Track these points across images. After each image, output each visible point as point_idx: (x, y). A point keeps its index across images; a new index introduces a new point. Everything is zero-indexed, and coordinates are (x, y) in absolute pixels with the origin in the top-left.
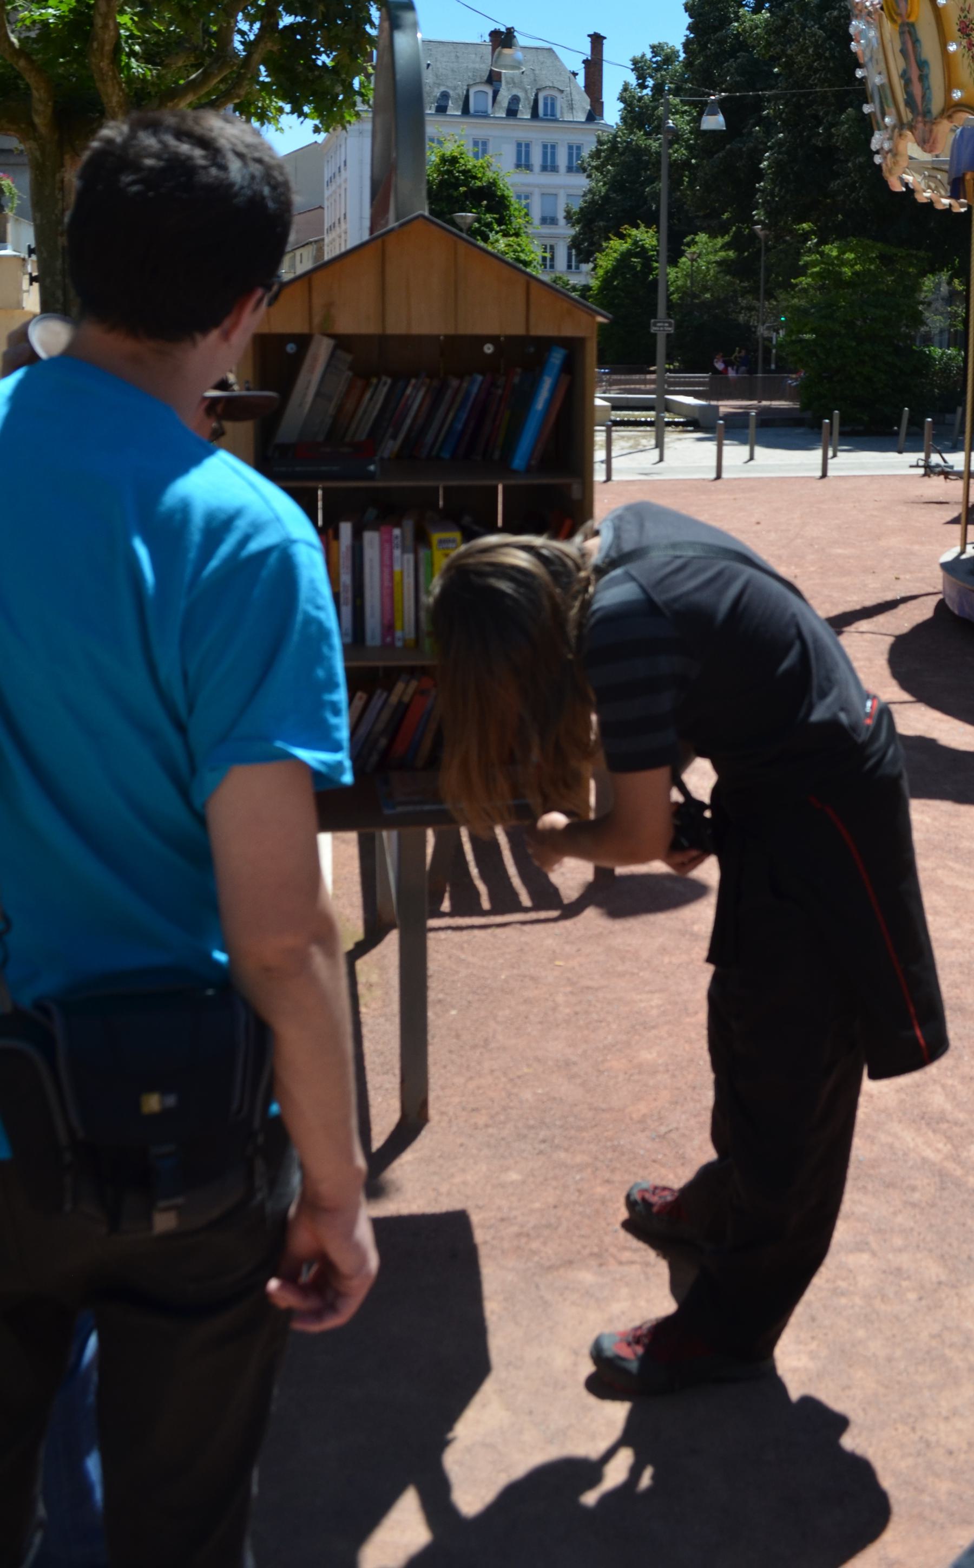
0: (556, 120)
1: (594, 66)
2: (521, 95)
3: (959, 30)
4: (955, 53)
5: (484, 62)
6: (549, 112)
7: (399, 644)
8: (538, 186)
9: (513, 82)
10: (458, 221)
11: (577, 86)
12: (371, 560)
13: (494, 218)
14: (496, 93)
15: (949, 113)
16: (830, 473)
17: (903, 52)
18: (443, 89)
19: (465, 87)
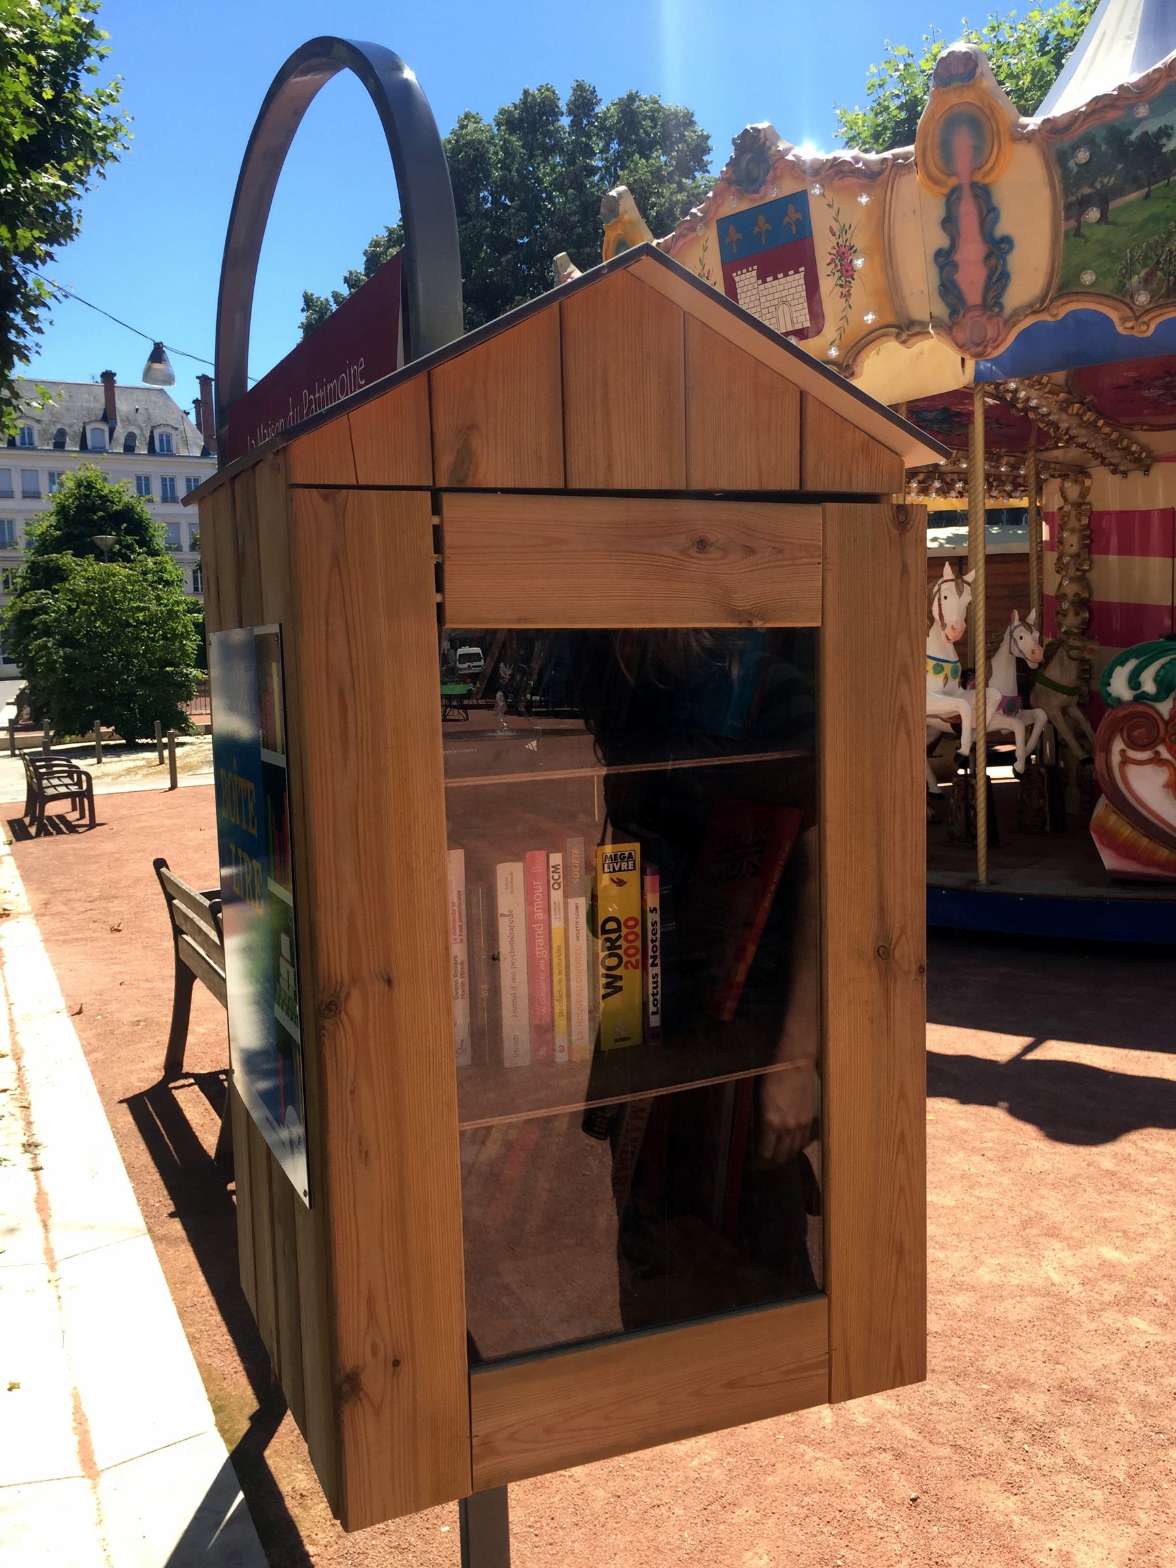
0: (173, 455)
2: (137, 432)
5: (98, 402)
7: (561, 1057)
9: (128, 421)
10: (98, 543)
11: (189, 423)
12: (510, 915)
13: (135, 540)
14: (112, 431)
16: (179, 784)
18: (59, 426)
19: (81, 425)
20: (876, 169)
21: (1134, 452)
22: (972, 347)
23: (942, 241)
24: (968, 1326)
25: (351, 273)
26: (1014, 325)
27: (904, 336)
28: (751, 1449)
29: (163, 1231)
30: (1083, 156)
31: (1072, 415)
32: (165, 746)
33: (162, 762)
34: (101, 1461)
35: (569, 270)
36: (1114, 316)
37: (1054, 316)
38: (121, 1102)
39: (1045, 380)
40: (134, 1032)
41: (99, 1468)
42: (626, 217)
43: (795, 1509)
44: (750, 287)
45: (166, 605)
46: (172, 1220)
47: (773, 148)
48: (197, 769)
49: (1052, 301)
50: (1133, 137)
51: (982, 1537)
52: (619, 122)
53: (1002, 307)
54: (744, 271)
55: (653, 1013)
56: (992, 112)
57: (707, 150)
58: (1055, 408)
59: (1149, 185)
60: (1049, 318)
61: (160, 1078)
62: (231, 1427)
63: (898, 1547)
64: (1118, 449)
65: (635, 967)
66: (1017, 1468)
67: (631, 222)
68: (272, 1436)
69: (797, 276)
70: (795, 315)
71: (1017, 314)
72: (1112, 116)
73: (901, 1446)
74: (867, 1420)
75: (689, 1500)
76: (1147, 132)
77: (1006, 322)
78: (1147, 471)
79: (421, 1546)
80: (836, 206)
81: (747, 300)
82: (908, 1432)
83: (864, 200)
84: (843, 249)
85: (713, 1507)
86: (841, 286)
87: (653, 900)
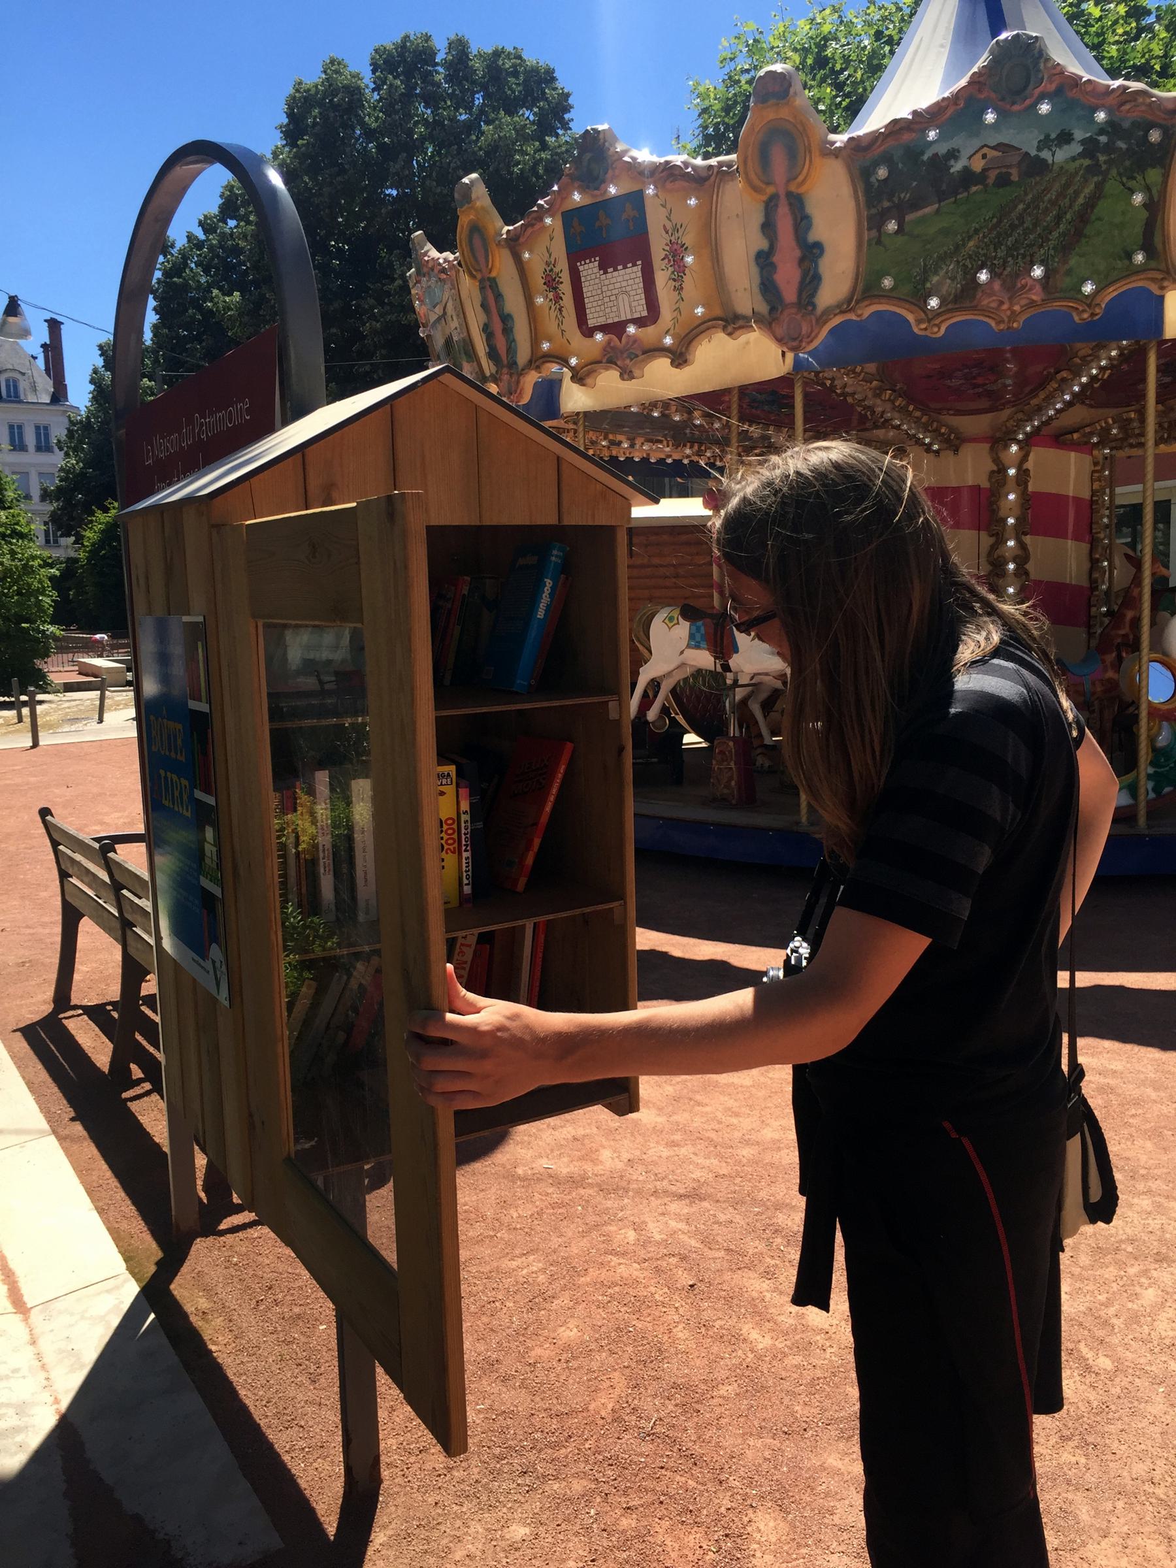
0: (20, 402)
1: (53, 351)
3: (545, 284)
4: (541, 306)
6: (12, 394)
8: (34, 465)
15: (537, 363)
16: (41, 743)
17: (484, 306)
20: (704, 174)
21: (943, 434)
22: (789, 341)
23: (764, 244)
24: (750, 1169)
25: (206, 217)
26: (825, 322)
27: (730, 329)
28: (569, 1260)
29: (66, 1132)
30: (882, 173)
31: (885, 401)
32: (25, 704)
33: (20, 720)
34: (29, 1301)
35: (426, 248)
36: (911, 318)
37: (859, 316)
38: (15, 1031)
39: (858, 369)
40: (18, 973)
41: (29, 1306)
42: (478, 204)
43: (600, 1298)
44: (593, 276)
45: (20, 560)
46: (74, 1123)
47: (612, 149)
48: (57, 728)
49: (857, 302)
50: (925, 157)
51: (740, 1307)
52: (483, 77)
53: (814, 306)
54: (588, 261)
55: (467, 884)
56: (804, 130)
57: (567, 109)
58: (870, 394)
59: (940, 202)
60: (854, 318)
61: (50, 1010)
62: (140, 1271)
63: (676, 1318)
64: (930, 432)
65: (453, 852)
66: (773, 1262)
67: (483, 208)
68: (176, 1275)
69: (635, 269)
70: (634, 304)
71: (829, 312)
72: (907, 137)
73: (686, 1252)
74: (662, 1236)
75: (518, 1297)
76: (937, 154)
77: (817, 320)
78: (956, 450)
79: (303, 1339)
80: (668, 206)
81: (591, 288)
82: (693, 1243)
83: (692, 202)
84: (675, 247)
85: (537, 1300)
86: (674, 280)
87: (465, 806)
